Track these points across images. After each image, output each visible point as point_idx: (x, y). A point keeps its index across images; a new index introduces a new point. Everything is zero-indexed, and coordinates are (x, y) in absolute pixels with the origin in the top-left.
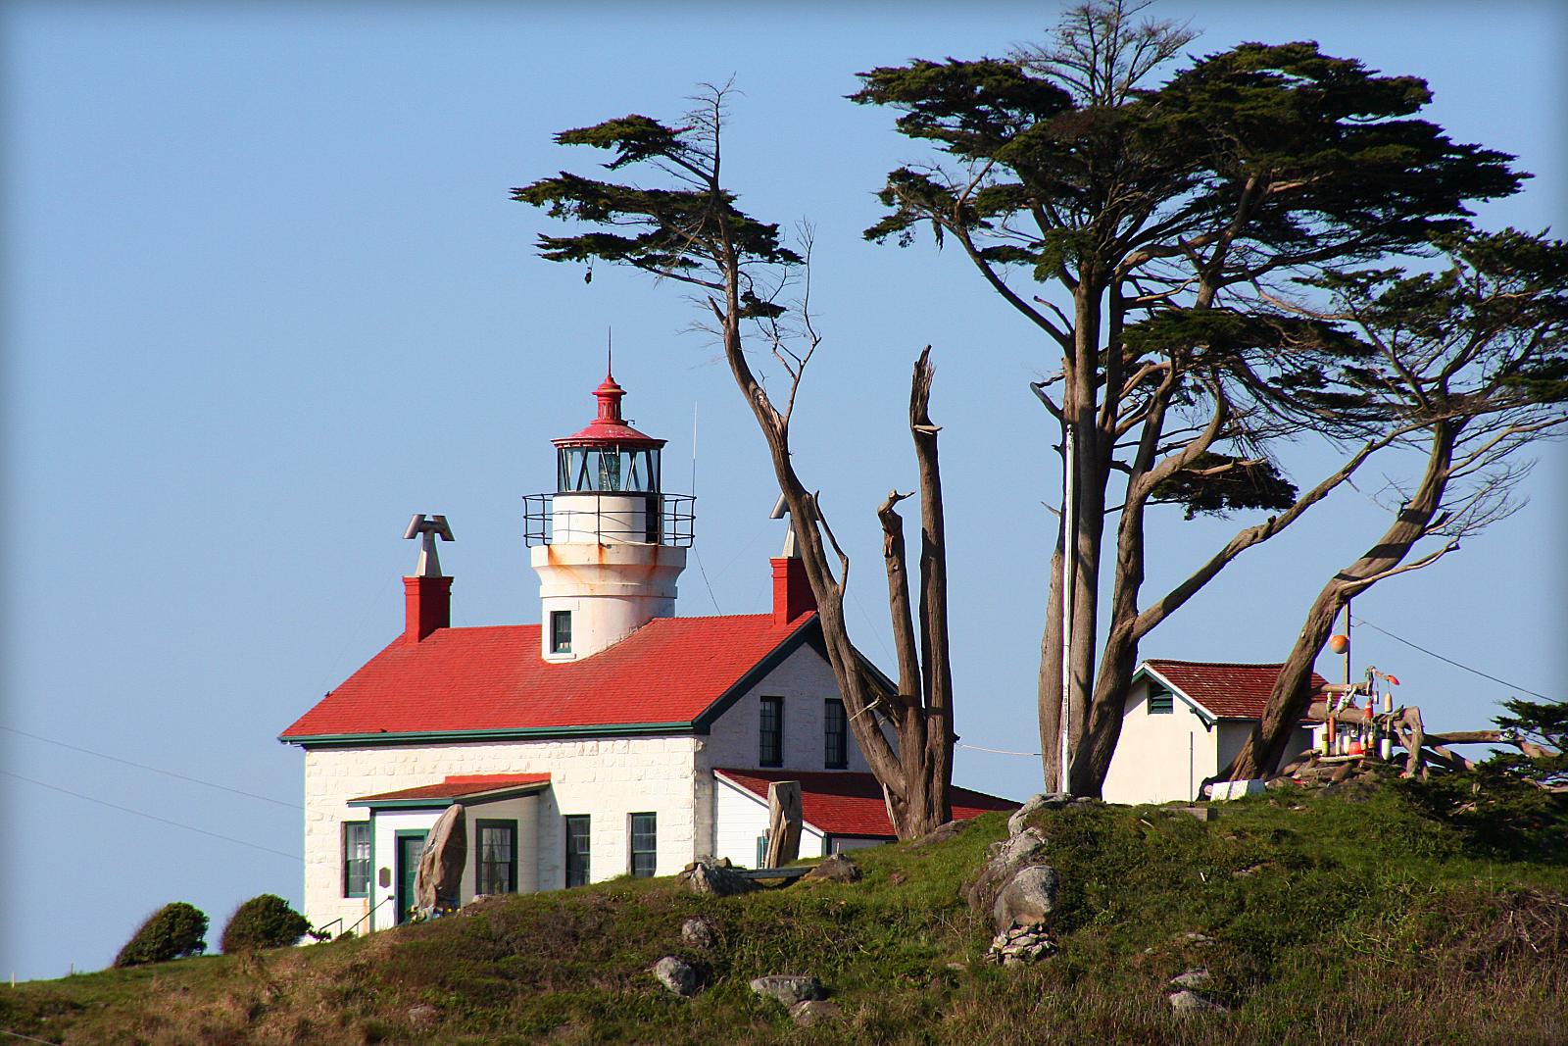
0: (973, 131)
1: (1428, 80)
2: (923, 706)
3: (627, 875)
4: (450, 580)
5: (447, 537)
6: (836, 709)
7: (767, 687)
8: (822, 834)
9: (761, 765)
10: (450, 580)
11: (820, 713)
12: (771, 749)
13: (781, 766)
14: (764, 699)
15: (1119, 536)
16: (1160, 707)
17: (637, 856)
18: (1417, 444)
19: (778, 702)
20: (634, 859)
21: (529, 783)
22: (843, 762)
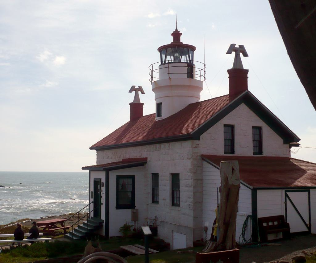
0: (88, 228)
1: (102, 197)
2: (214, 238)
3: (189, 248)
4: (143, 104)
5: (143, 93)
6: (258, 130)
7: (227, 120)
8: (144, 247)
9: (225, 153)
10: (143, 104)
11: (250, 132)
12: (257, 147)
13: (234, 154)
14: (225, 126)
15: (213, 225)
16: (146, 141)
17: (306, 193)
18: (288, 200)
19: (232, 127)
20: (270, 241)
21: (138, 161)
22: (261, 152)
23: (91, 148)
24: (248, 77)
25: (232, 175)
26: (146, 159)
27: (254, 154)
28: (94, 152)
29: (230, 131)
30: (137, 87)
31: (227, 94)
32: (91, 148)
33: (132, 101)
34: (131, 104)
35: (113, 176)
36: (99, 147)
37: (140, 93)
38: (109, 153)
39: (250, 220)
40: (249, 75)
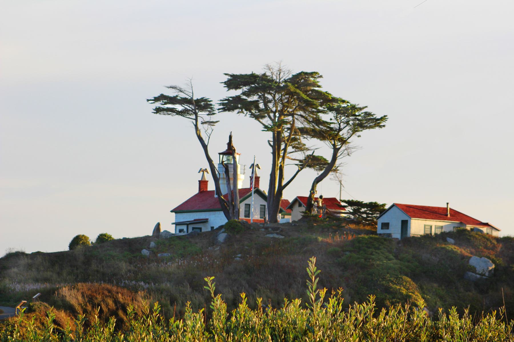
4: (207, 181)
14: (246, 204)
19: (249, 205)
23: (172, 211)
24: (77, 241)
25: (345, 175)
26: (207, 219)
27: (261, 218)
28: (174, 213)
29: (248, 207)
30: (204, 169)
31: (332, 152)
32: (172, 211)
33: (200, 179)
34: (199, 181)
35: (191, 227)
36: (176, 211)
37: (205, 173)
38: (180, 215)
39: (220, 300)
40: (260, 179)
